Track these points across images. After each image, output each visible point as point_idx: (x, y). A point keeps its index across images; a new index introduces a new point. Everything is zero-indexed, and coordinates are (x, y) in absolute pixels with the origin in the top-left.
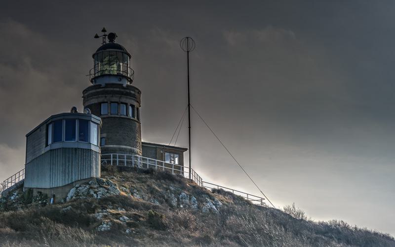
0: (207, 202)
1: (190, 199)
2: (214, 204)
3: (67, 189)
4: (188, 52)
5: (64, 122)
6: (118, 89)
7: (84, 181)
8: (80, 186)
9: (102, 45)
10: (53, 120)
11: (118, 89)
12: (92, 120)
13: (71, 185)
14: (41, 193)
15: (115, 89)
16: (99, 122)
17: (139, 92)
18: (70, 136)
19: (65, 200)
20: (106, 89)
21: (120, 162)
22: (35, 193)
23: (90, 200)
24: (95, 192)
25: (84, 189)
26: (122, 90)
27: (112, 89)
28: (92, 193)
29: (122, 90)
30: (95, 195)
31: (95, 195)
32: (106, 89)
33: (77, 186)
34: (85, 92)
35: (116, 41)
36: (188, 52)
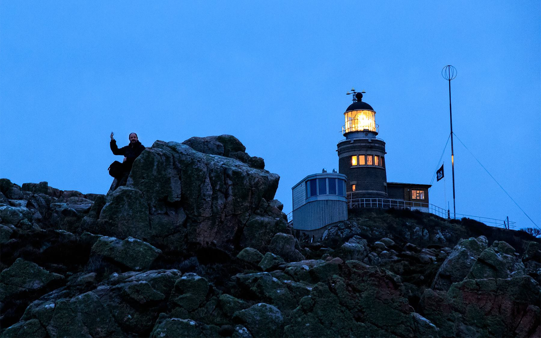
0: (438, 233)
1: (423, 232)
2: (443, 235)
3: (322, 231)
4: (450, 80)
5: (327, 180)
6: (364, 144)
7: (334, 225)
8: (331, 228)
9: (352, 102)
10: (309, 179)
11: (364, 144)
12: (371, 164)
13: (325, 228)
14: (304, 233)
15: (362, 144)
16: (344, 178)
17: (383, 143)
18: (323, 192)
19: (321, 239)
20: (355, 145)
21: (361, 204)
22: (301, 234)
23: (337, 237)
24: (342, 233)
25: (333, 230)
26: (368, 144)
27: (359, 144)
28: (339, 233)
29: (368, 144)
30: (341, 235)
31: (341, 235)
32: (355, 145)
33: (329, 228)
34: (339, 145)
35: (363, 100)
36: (450, 80)
